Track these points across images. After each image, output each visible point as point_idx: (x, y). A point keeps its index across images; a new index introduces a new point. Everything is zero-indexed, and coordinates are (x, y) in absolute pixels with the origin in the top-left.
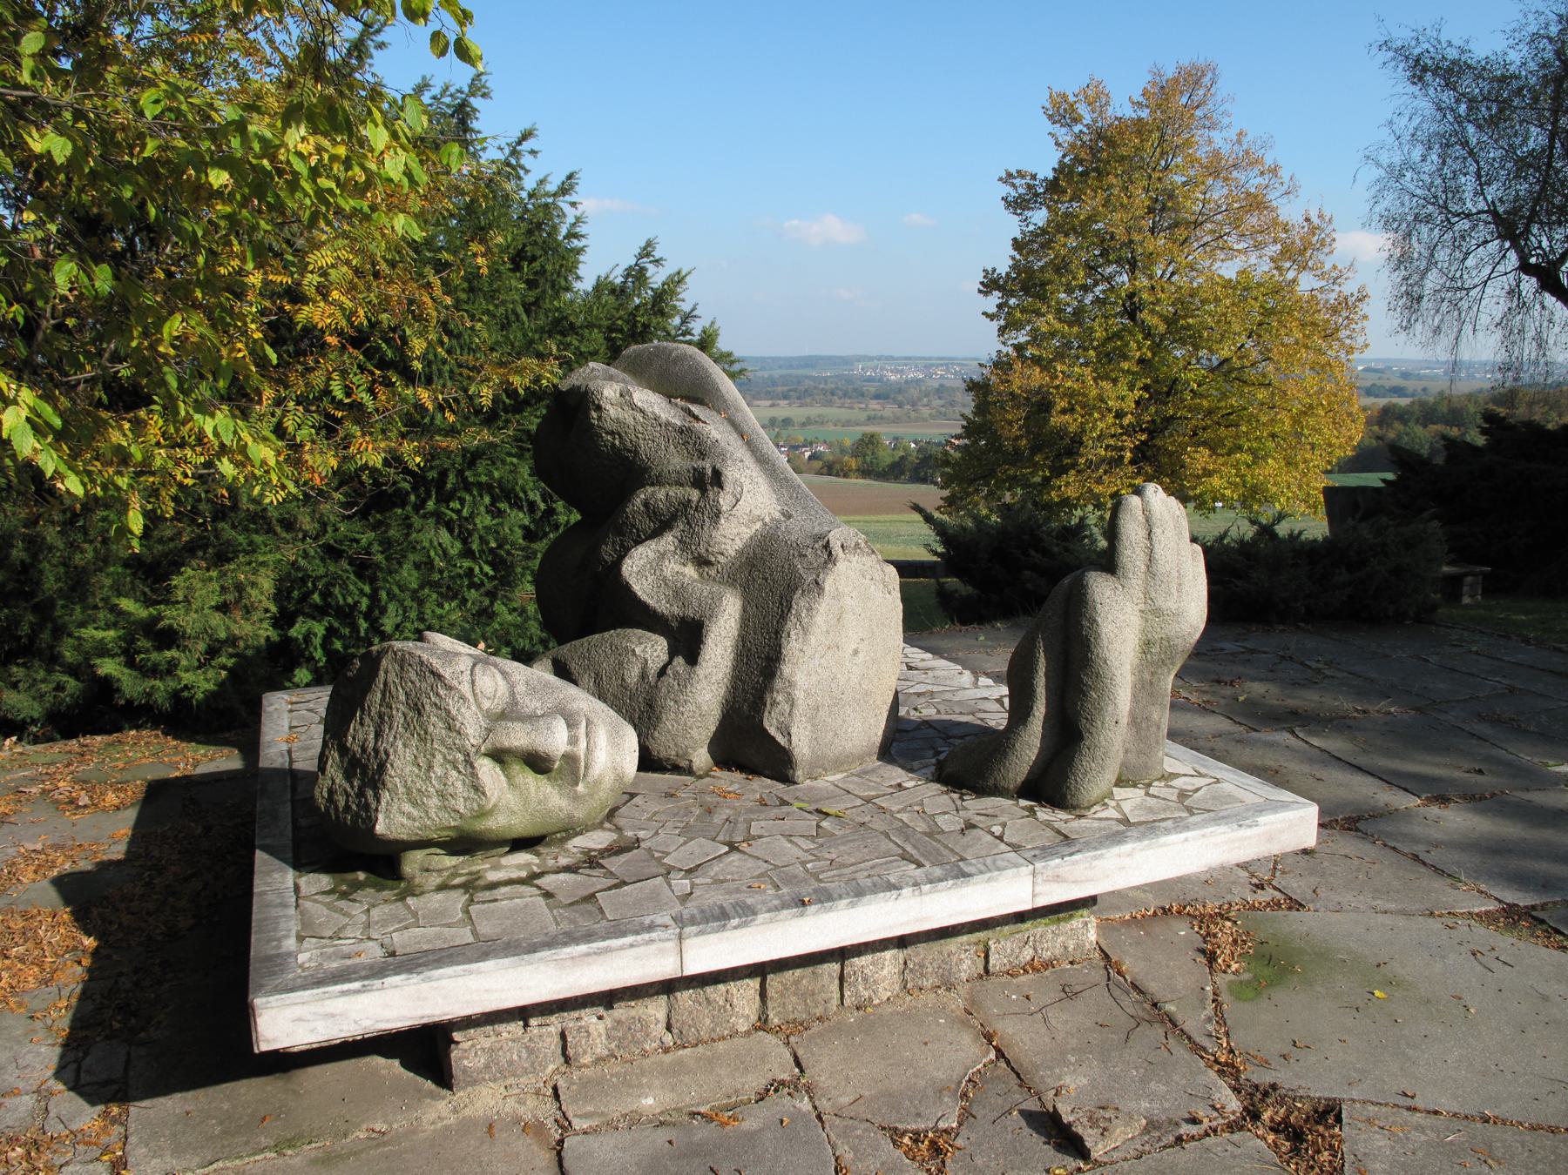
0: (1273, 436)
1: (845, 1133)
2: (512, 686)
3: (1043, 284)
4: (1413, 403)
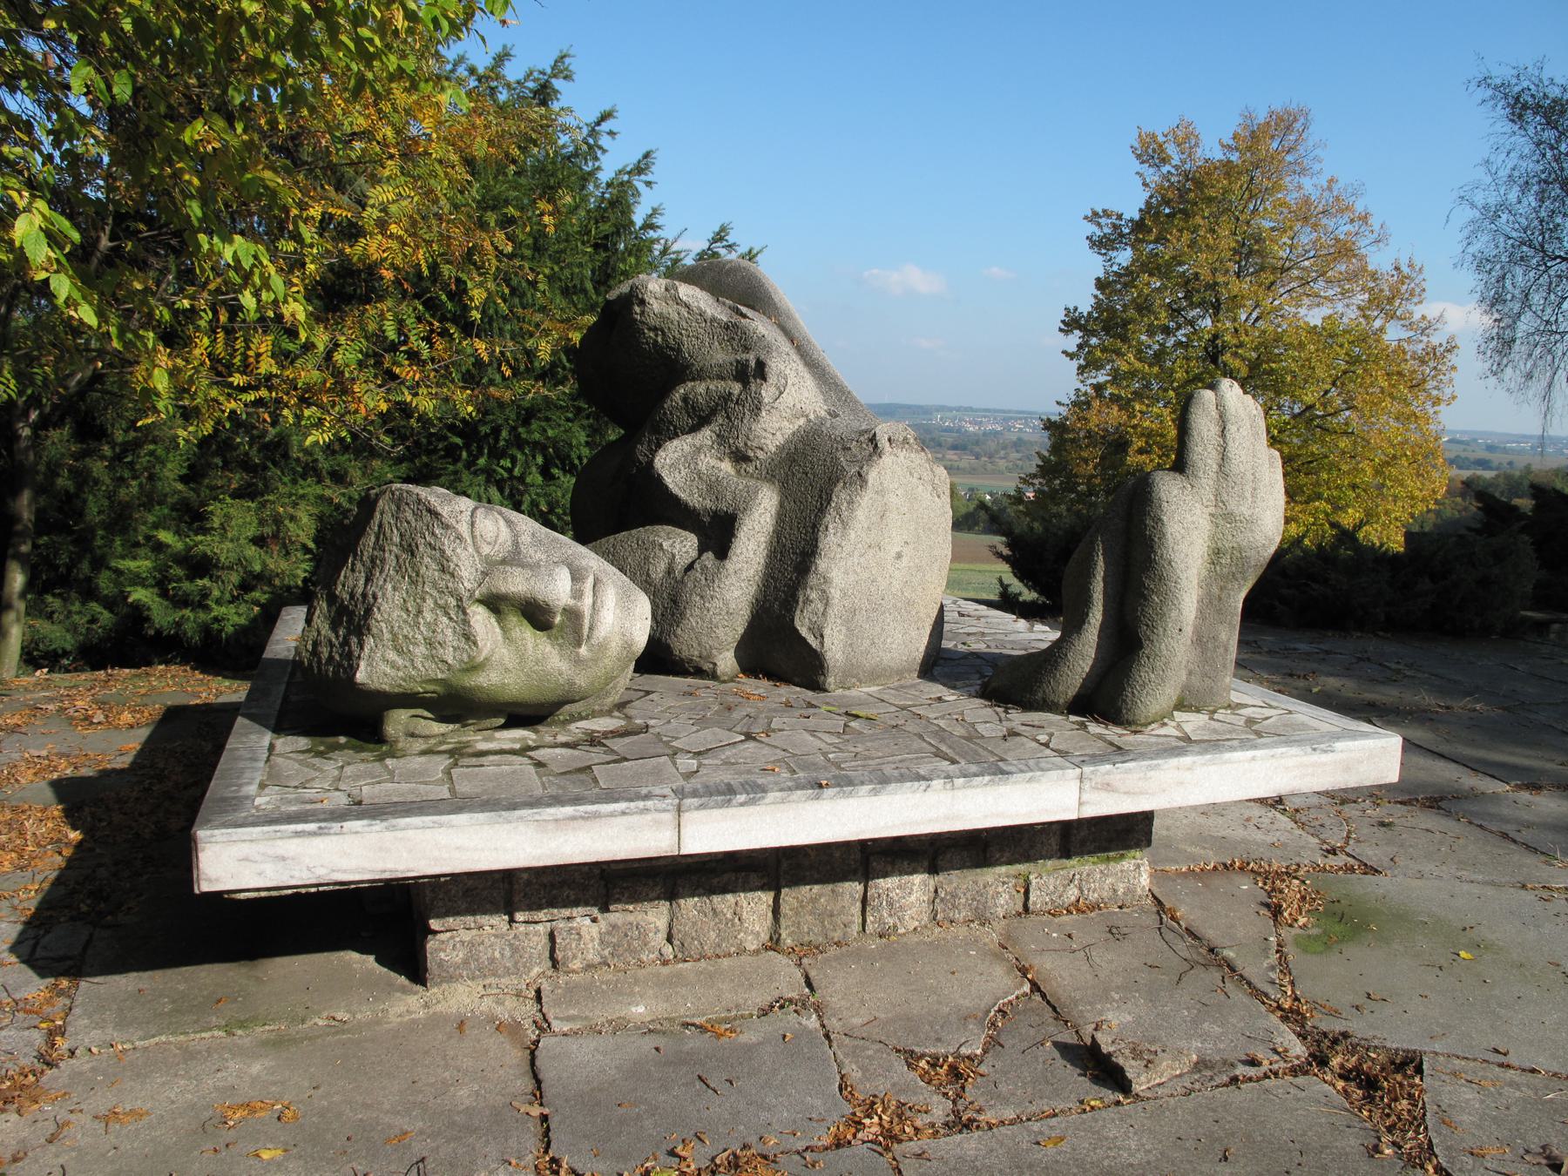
0: (1354, 487)
1: (854, 1053)
3: (1125, 323)
4: (1498, 476)
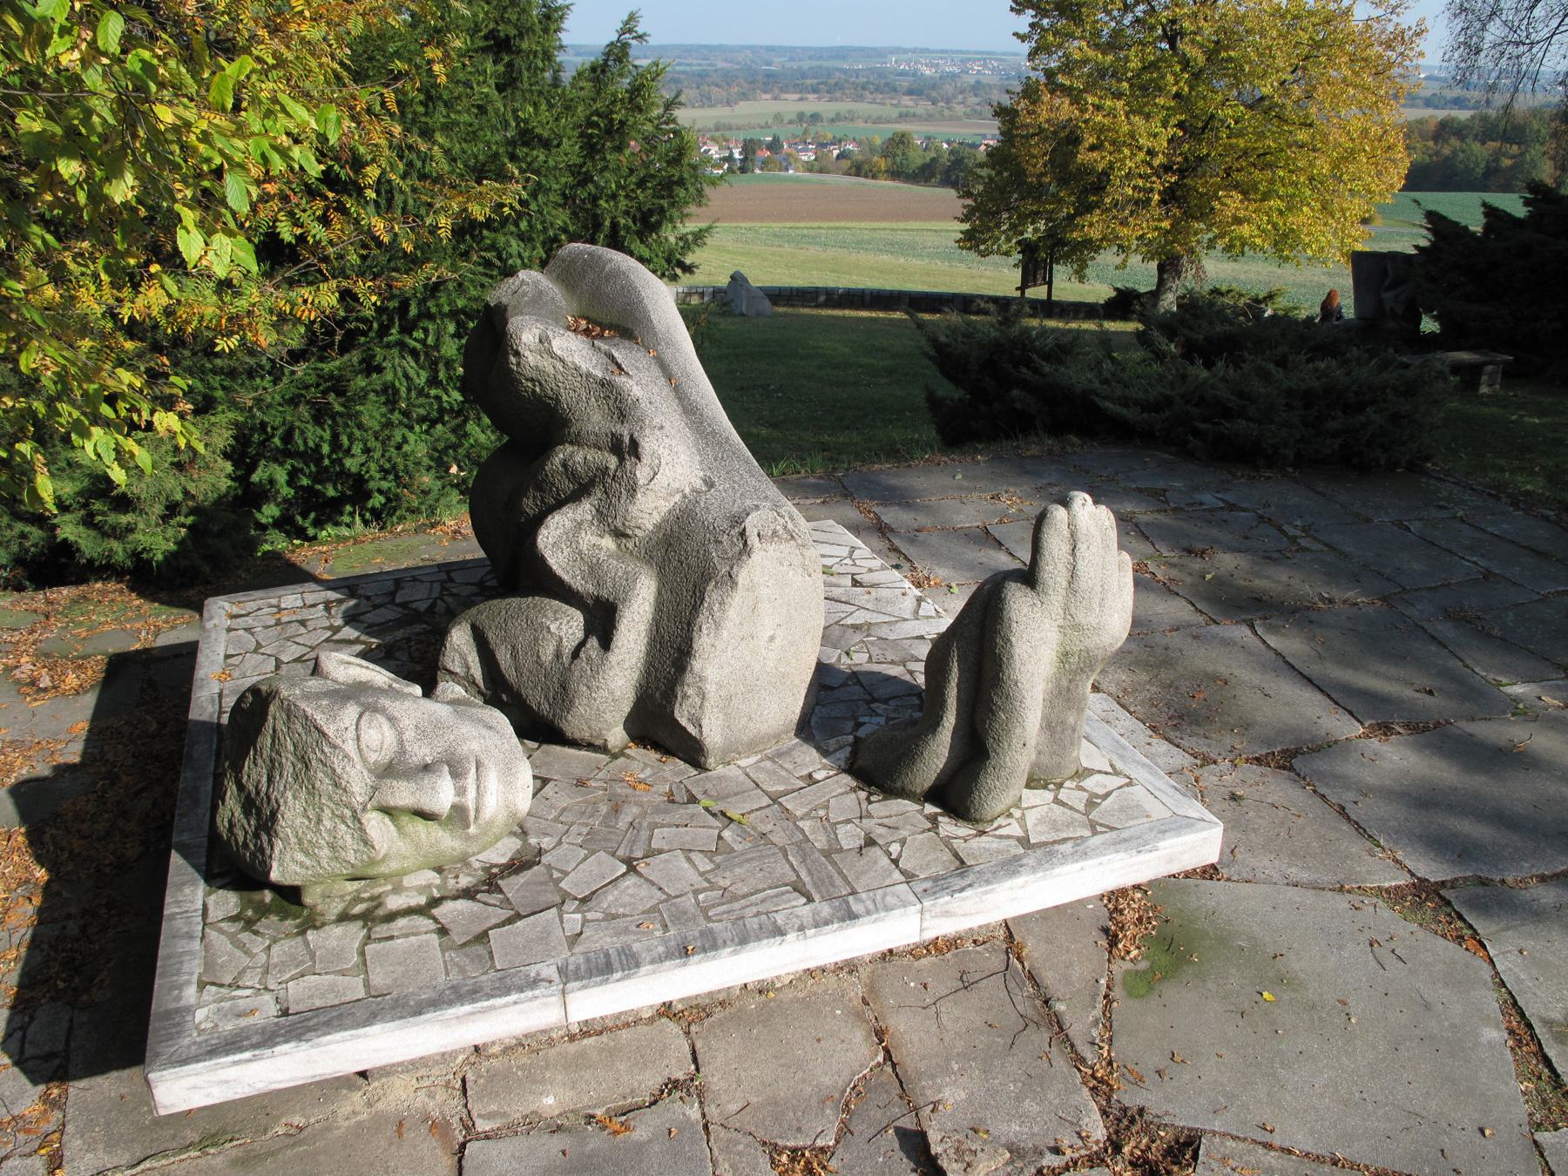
2: (400, 734)
4: (1473, 117)
